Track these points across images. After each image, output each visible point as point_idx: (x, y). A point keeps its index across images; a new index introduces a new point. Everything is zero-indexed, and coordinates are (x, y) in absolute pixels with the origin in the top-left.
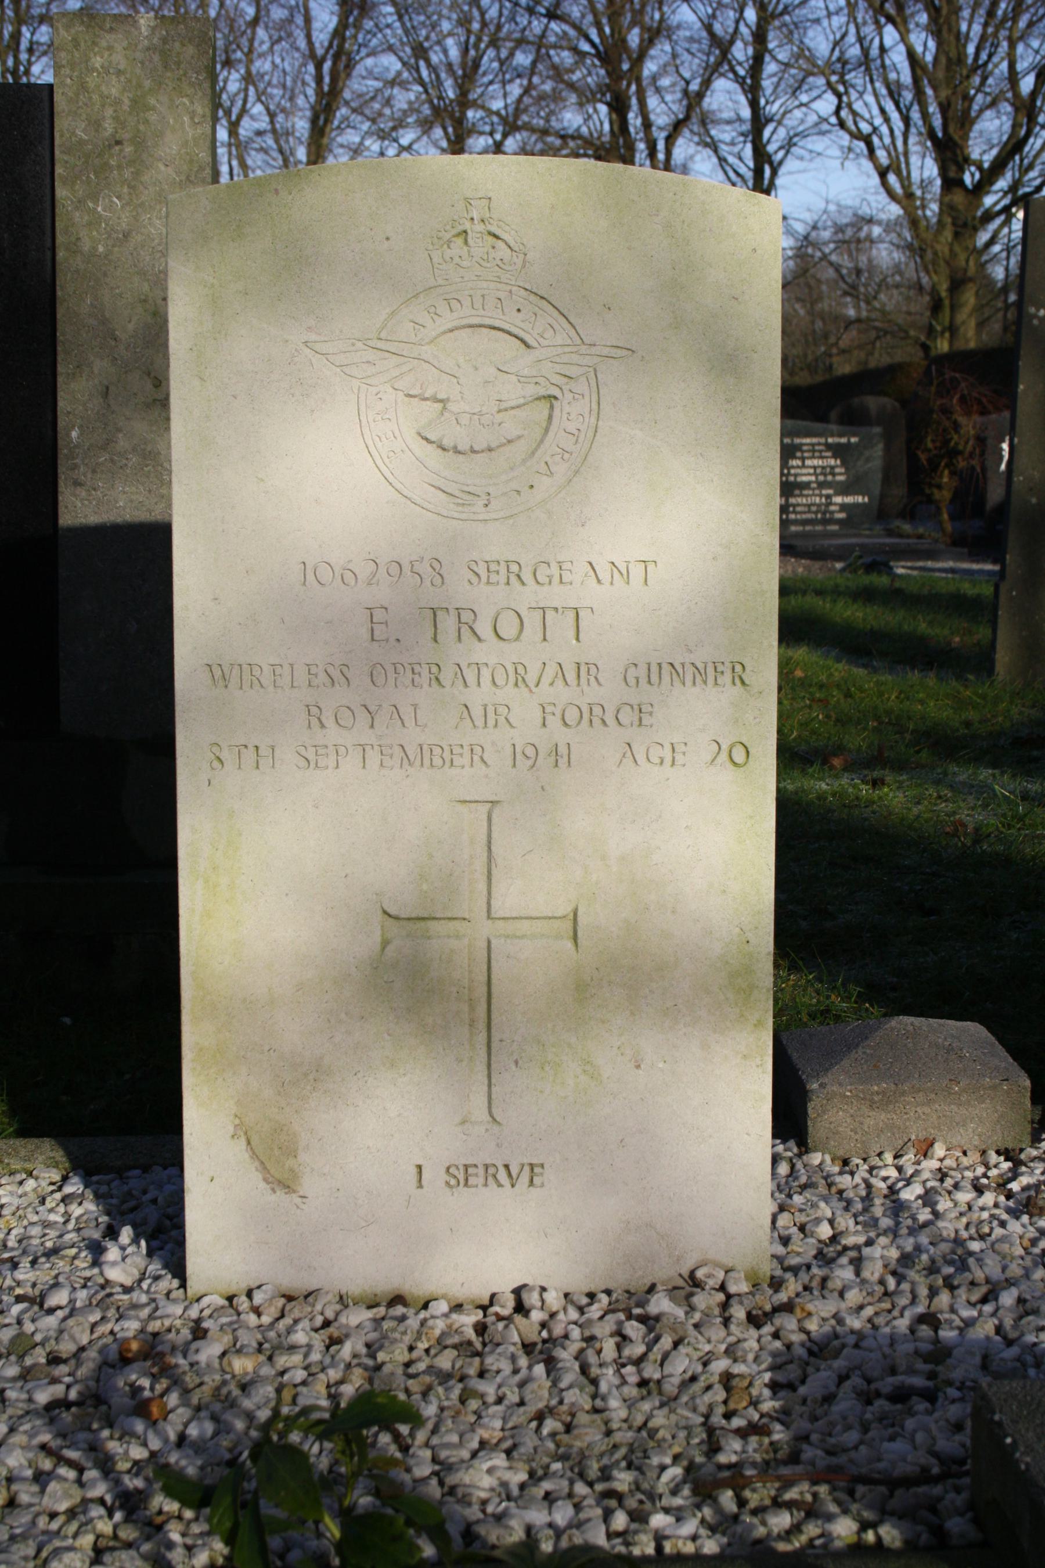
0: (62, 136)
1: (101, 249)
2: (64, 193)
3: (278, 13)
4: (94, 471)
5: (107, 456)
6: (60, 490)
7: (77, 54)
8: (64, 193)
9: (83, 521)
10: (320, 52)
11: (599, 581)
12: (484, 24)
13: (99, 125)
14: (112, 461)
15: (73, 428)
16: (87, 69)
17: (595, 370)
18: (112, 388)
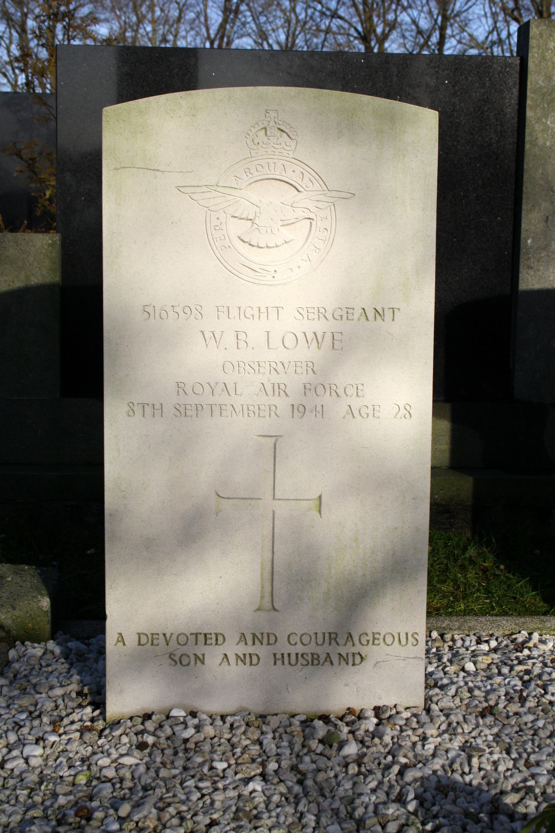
0: (531, 84)
1: (548, 144)
2: (531, 114)
3: (191, 15)
4: (538, 261)
5: (546, 253)
6: (520, 270)
7: (541, 41)
8: (531, 114)
9: (532, 287)
10: (212, 36)
11: (367, 319)
12: (298, 21)
13: (551, 78)
14: (548, 256)
15: (529, 238)
16: (546, 48)
17: (334, 205)
18: (550, 218)
